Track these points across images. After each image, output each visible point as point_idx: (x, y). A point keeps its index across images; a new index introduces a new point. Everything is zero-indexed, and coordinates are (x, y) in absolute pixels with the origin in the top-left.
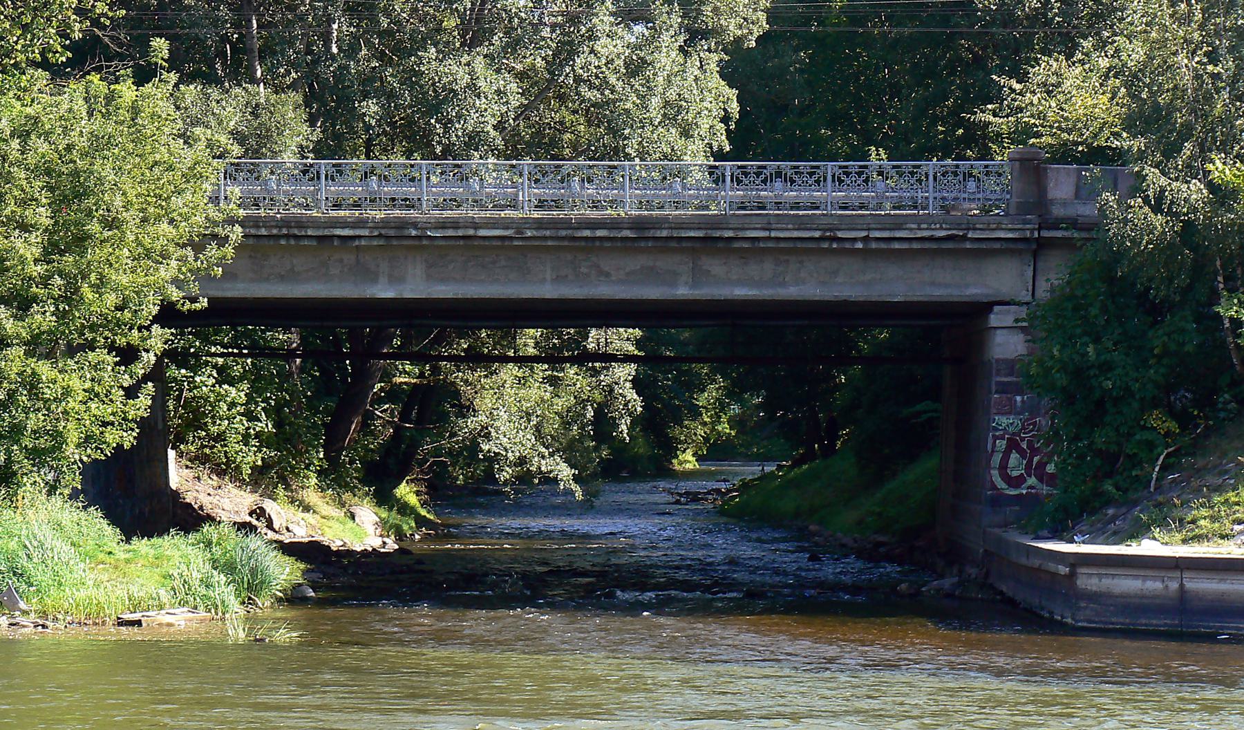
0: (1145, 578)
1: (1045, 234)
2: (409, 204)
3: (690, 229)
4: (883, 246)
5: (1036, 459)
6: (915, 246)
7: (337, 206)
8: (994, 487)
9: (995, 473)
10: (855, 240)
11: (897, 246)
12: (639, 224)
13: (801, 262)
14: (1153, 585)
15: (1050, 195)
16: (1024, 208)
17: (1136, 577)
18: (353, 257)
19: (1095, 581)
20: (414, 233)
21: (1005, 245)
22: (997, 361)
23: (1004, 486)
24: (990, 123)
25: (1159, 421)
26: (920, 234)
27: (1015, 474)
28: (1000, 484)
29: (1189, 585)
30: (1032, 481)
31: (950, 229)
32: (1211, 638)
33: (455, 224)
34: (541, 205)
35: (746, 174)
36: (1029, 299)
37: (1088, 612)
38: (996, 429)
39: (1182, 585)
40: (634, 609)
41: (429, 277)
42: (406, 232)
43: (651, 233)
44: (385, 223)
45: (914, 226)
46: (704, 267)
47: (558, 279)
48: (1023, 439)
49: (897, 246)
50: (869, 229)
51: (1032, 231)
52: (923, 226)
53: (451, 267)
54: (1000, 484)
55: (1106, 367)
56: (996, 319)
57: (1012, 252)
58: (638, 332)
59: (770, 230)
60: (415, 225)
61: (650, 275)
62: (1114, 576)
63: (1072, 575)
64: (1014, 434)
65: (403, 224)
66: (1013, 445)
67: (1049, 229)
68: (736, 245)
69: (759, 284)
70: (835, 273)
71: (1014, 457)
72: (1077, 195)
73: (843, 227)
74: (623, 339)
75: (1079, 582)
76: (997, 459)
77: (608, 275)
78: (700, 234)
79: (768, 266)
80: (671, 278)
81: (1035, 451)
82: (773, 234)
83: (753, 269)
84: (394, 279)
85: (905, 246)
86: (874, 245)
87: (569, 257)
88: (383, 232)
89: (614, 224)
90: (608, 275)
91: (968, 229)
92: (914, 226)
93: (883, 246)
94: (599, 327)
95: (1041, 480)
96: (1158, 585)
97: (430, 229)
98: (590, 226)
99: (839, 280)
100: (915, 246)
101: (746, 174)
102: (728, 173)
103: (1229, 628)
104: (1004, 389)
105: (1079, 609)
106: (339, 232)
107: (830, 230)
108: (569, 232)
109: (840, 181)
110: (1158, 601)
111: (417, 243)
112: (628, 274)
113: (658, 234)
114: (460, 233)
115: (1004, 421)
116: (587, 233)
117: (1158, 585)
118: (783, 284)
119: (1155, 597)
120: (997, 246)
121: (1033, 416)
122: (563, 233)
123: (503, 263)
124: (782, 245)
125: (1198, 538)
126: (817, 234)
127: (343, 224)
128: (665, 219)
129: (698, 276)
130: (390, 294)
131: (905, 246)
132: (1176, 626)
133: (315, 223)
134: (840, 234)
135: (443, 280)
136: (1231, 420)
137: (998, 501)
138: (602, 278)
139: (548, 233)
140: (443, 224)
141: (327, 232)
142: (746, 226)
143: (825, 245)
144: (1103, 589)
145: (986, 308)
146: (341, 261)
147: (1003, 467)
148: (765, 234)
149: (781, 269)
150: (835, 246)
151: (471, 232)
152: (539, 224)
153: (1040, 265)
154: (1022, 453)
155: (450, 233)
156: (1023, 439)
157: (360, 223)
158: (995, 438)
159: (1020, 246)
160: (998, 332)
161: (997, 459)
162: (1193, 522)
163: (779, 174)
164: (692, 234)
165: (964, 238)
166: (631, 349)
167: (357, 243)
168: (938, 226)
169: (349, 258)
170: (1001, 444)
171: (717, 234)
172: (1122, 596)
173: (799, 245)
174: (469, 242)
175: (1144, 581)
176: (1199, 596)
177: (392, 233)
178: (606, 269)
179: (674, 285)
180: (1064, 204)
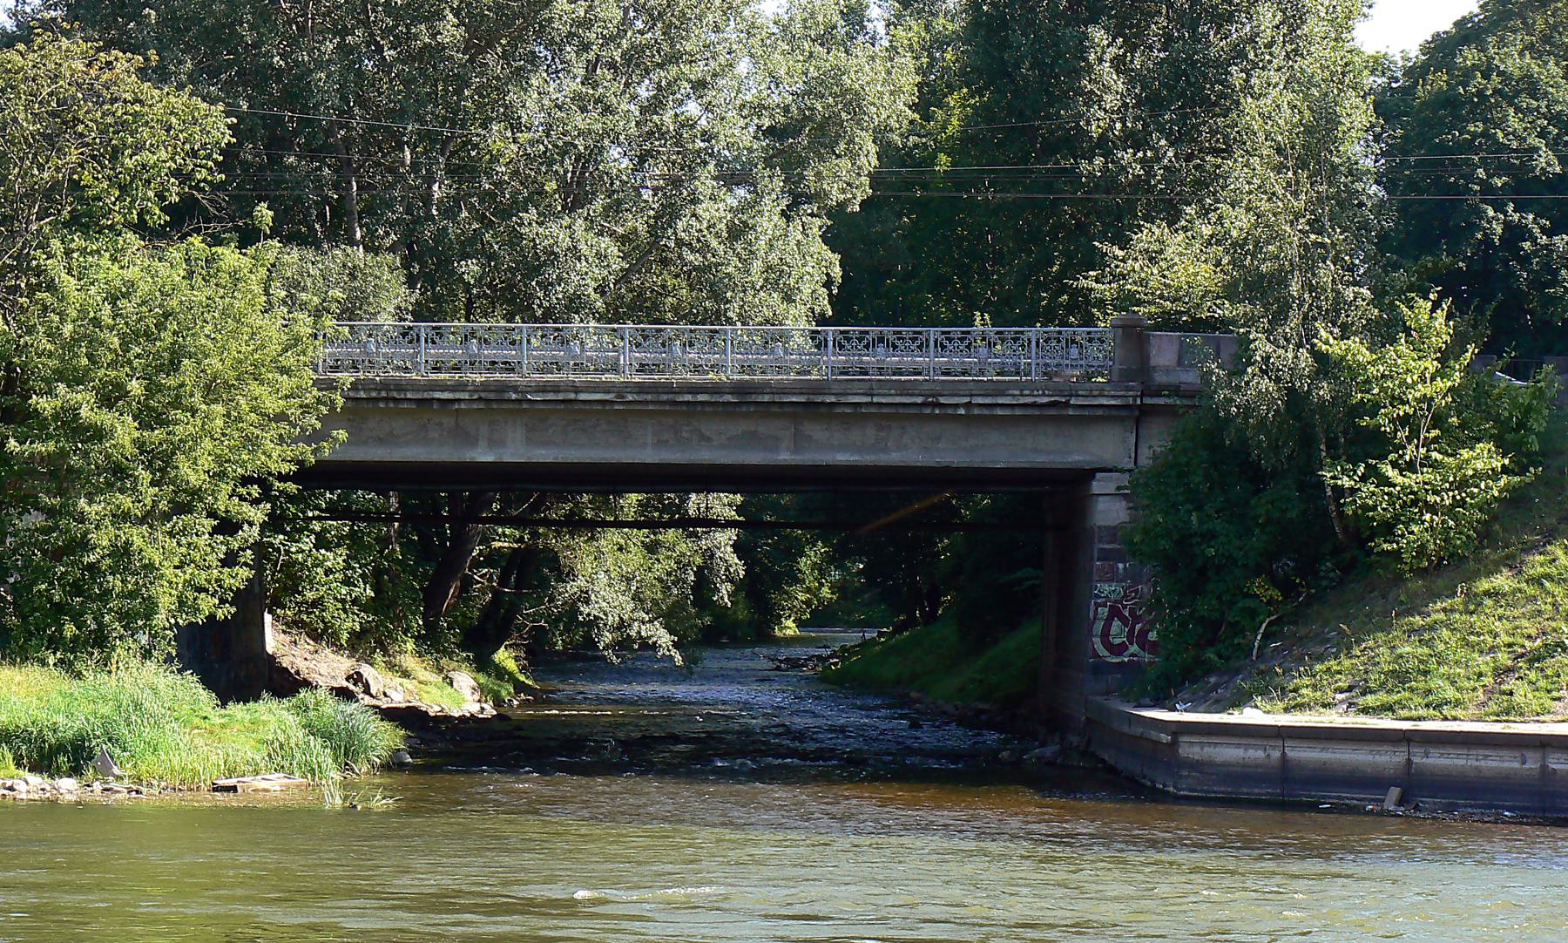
0: (1247, 747)
1: (1148, 401)
2: (509, 367)
4: (986, 412)
5: (1138, 627)
6: (1018, 412)
7: (436, 369)
8: (1095, 654)
9: (1097, 640)
10: (957, 406)
11: (999, 412)
12: (740, 389)
15: (1153, 362)
16: (1127, 375)
17: (1238, 746)
19: (1196, 749)
20: (514, 396)
21: (1107, 412)
23: (1106, 653)
25: (1261, 588)
26: (1022, 401)
27: (1117, 641)
28: (1102, 652)
29: (1291, 754)
30: (1134, 648)
31: (1052, 396)
32: (1313, 807)
33: (555, 388)
34: (642, 368)
36: (1131, 465)
38: (1098, 596)
39: (1284, 754)
41: (529, 441)
42: (506, 396)
43: (753, 398)
44: (485, 386)
46: (806, 433)
47: (660, 444)
48: (1125, 607)
49: (999, 412)
50: (971, 395)
51: (1135, 397)
52: (1027, 392)
53: (550, 431)
54: (1102, 652)
55: (1210, 536)
57: (1122, 420)
58: (739, 498)
59: (872, 395)
60: (515, 389)
61: (752, 439)
63: (1174, 744)
64: (1116, 601)
65: (503, 387)
66: (1115, 613)
67: (1151, 396)
68: (838, 410)
70: (938, 439)
71: (1116, 623)
72: (1180, 363)
73: (945, 393)
74: (723, 504)
75: (1180, 751)
76: (1099, 627)
77: (709, 439)
78: (802, 399)
79: (871, 432)
81: (1137, 619)
82: (875, 400)
83: (855, 435)
84: (494, 443)
85: (1008, 412)
86: (976, 411)
87: (671, 421)
88: (483, 395)
89: (715, 389)
90: (709, 439)
91: (1071, 396)
93: (986, 412)
94: (697, 492)
95: (1142, 648)
96: (1260, 754)
98: (693, 390)
100: (1018, 412)
103: (1330, 797)
104: (1105, 556)
105: (1181, 777)
106: (437, 395)
109: (943, 347)
112: (728, 439)
113: (760, 399)
114: (561, 396)
115: (1107, 588)
116: (688, 398)
117: (1260, 754)
118: (885, 450)
120: (1100, 412)
122: (665, 397)
125: (1300, 707)
126: (919, 400)
127: (442, 386)
128: (767, 384)
129: (799, 442)
130: (490, 459)
131: (1008, 412)
134: (942, 400)
135: (545, 444)
136: (1333, 588)
137: (1100, 668)
138: (703, 443)
140: (543, 388)
141: (426, 395)
142: (849, 391)
143: (928, 411)
144: (1206, 758)
146: (441, 424)
147: (1105, 635)
149: (883, 434)
150: (937, 412)
151: (572, 396)
152: (641, 388)
153: (1143, 432)
154: (1124, 620)
155: (550, 396)
156: (1125, 607)
157: (460, 386)
158: (1097, 605)
159: (1124, 413)
160: (1101, 499)
161: (1099, 627)
165: (1067, 404)
166: (731, 514)
168: (1040, 392)
169: (448, 421)
170: (1104, 612)
172: (1223, 765)
176: (1299, 764)
177: (492, 396)
180: (1167, 371)
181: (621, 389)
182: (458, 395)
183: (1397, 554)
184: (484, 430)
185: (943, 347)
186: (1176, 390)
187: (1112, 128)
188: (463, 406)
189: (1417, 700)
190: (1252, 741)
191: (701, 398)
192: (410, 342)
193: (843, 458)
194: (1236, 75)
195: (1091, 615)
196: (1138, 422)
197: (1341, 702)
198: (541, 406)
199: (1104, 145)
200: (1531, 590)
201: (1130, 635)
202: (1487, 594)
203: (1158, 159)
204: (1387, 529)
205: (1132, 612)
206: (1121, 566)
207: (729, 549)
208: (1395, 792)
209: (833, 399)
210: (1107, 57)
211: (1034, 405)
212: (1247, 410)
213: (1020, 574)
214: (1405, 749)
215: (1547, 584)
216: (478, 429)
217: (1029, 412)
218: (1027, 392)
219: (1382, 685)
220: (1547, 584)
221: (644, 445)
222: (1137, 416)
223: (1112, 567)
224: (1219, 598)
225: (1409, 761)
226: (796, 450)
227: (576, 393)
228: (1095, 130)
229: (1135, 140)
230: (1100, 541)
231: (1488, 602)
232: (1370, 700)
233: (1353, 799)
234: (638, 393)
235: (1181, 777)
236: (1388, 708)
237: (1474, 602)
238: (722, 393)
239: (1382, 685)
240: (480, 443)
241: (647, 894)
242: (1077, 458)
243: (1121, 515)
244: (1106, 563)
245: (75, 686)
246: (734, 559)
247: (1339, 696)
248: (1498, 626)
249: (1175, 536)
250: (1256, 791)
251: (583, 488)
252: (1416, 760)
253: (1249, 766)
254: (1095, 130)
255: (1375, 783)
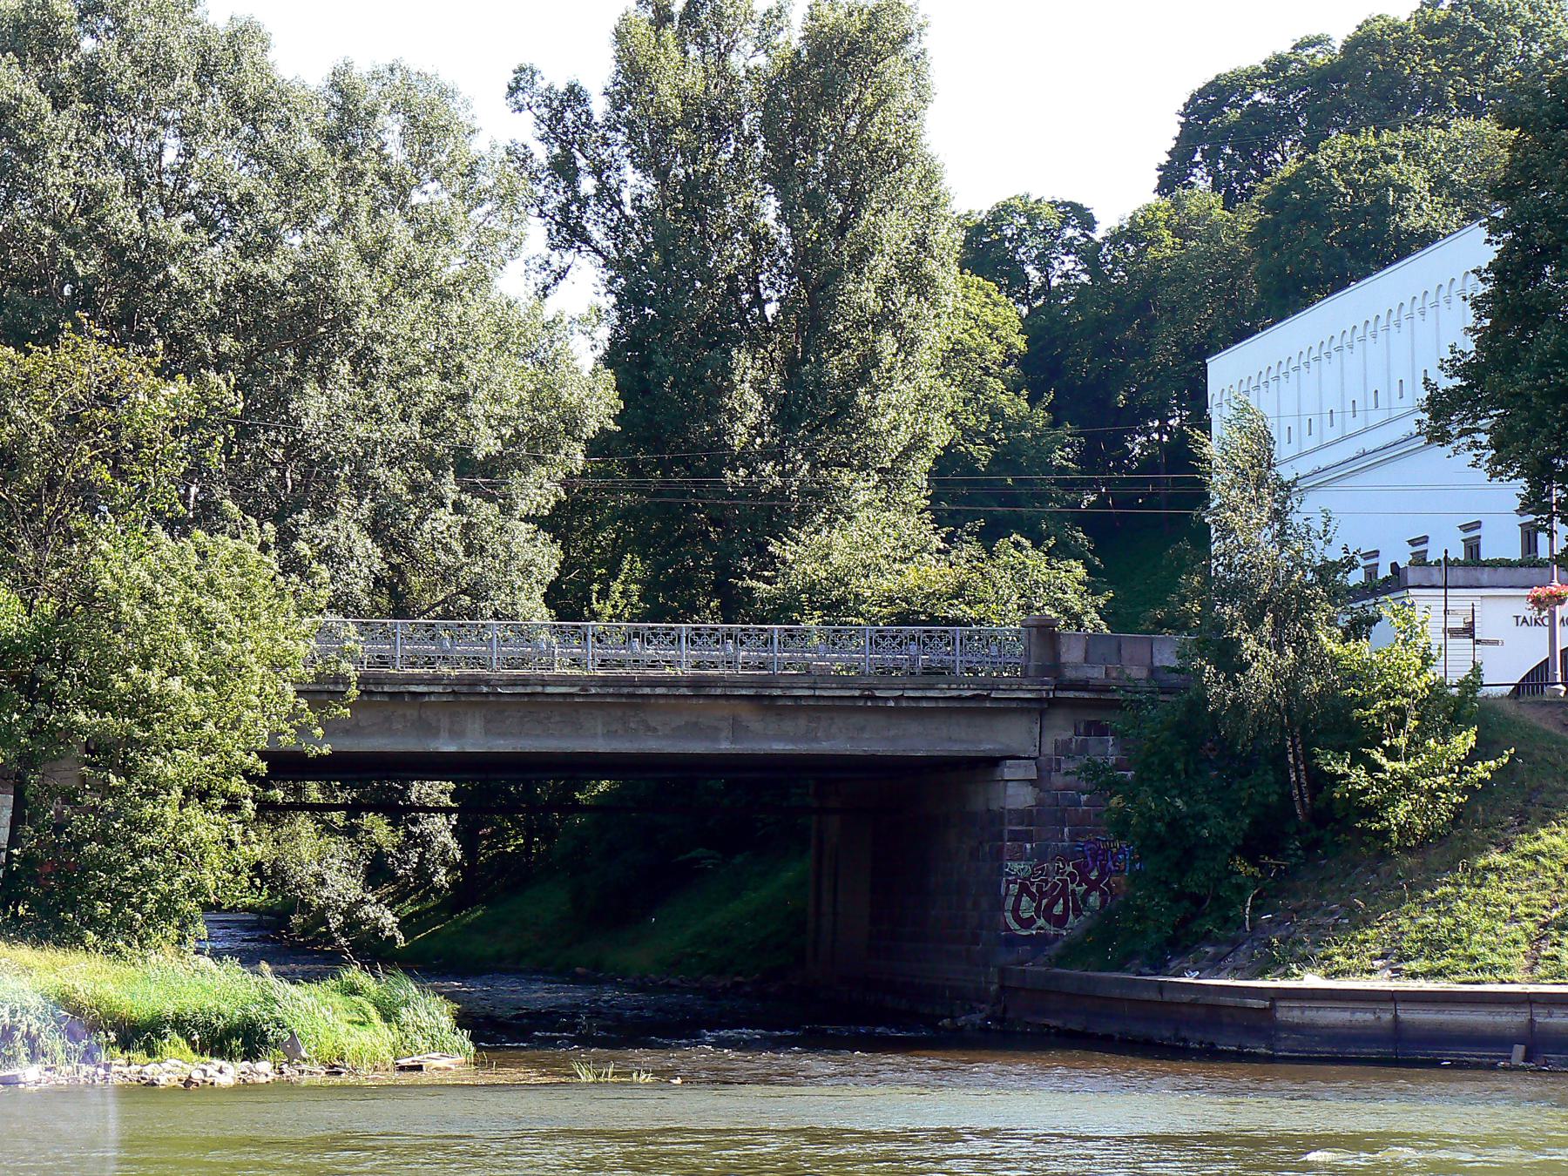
0: (1354, 1011)
1: (1059, 694)
2: (476, 661)
3: (742, 687)
4: (913, 704)
5: (1044, 902)
6: (941, 704)
7: (413, 665)
8: (1008, 928)
9: (1008, 915)
10: (887, 699)
11: (924, 704)
12: (696, 684)
13: (832, 719)
14: (1363, 1016)
15: (1063, 660)
16: (1043, 670)
17: (1344, 1010)
18: (416, 714)
19: (1297, 1013)
20: (485, 689)
21: (1020, 705)
22: (1009, 810)
23: (1017, 927)
24: (753, 589)
25: (1242, 867)
27: (1026, 915)
28: (1014, 926)
29: (1403, 1016)
30: (1041, 922)
32: (1434, 1064)
33: (525, 681)
34: (603, 664)
35: (655, 635)
36: (1036, 754)
37: (1289, 1042)
38: (1008, 874)
39: (1396, 1016)
40: (550, 1042)
41: (487, 732)
42: (478, 689)
43: (707, 691)
44: (460, 680)
45: (945, 686)
47: (611, 734)
48: (1032, 883)
49: (924, 704)
50: (904, 689)
51: (1048, 691)
52: (954, 686)
53: (508, 722)
54: (1014, 926)
55: (1202, 818)
56: (1010, 771)
57: (1029, 711)
58: (451, 786)
59: (814, 689)
60: (487, 683)
61: (695, 730)
62: (1318, 1008)
63: (1273, 1008)
64: (1025, 879)
65: (475, 681)
66: (1024, 889)
67: (1062, 690)
68: (780, 703)
69: (793, 740)
70: (863, 729)
71: (1025, 899)
72: (1086, 660)
74: (435, 791)
75: (1278, 1015)
76: (1010, 902)
77: (655, 730)
78: (751, 692)
79: (802, 722)
80: (713, 733)
81: (1043, 894)
82: (817, 693)
83: (788, 726)
84: (455, 734)
85: (932, 704)
86: (904, 704)
87: (619, 713)
88: (456, 689)
89: (674, 683)
91: (992, 690)
92: (945, 686)
93: (913, 704)
94: (422, 780)
95: (1048, 921)
96: (1369, 1017)
97: (500, 686)
99: (866, 736)
100: (941, 704)
101: (700, 636)
102: (776, 636)
103: (1447, 1055)
104: (1016, 837)
105: (1279, 1039)
106: (413, 688)
107: (868, 689)
108: (631, 690)
109: (877, 644)
110: (1369, 1031)
111: (484, 699)
112: (673, 729)
113: (713, 692)
114: (529, 690)
115: (1016, 866)
116: (647, 691)
117: (1369, 1017)
118: (816, 739)
119: (1365, 1027)
120: (1014, 705)
121: (1042, 861)
122: (625, 691)
123: (558, 718)
124: (822, 703)
125: (1336, 974)
126: (857, 693)
127: (420, 681)
128: (720, 678)
129: (738, 729)
130: (453, 749)
131: (932, 704)
132: (1392, 1054)
133: (392, 680)
134: (877, 693)
135: (503, 735)
136: (1303, 864)
137: (1012, 941)
139: (611, 690)
140: (513, 682)
141: (402, 689)
143: (861, 703)
144: (1307, 1020)
145: (993, 762)
146: (404, 716)
147: (1016, 910)
148: (807, 693)
150: (869, 704)
151: (539, 689)
152: (604, 682)
153: (1044, 722)
154: (1031, 895)
155: (519, 690)
156: (1032, 883)
157: (436, 680)
158: (1009, 883)
159: (1034, 705)
160: (1010, 784)
161: (1010, 902)
162: (1329, 958)
163: (730, 636)
164: (744, 692)
165: (987, 697)
166: (446, 800)
167: (427, 699)
169: (412, 713)
170: (1014, 888)
171: (767, 692)
172: (1327, 1027)
173: (837, 703)
174: (533, 699)
175: (1353, 1013)
176: (1412, 1025)
177: (465, 689)
178: (653, 724)
179: (716, 740)
180: (1076, 667)
181: (584, 683)
182: (432, 689)
183: (1385, 832)
184: (445, 722)
185: (877, 644)
186: (1083, 685)
187: (753, 443)
188: (433, 699)
189: (1463, 965)
190: (1357, 1005)
191: (659, 691)
192: (717, 642)
193: (779, 747)
194: (863, 399)
195: (1003, 891)
196: (1042, 714)
197: (1382, 968)
198: (507, 699)
199: (745, 459)
200: (1529, 865)
201: (1037, 909)
202: (1487, 869)
203: (794, 472)
204: (1371, 812)
205: (1039, 888)
206: (1028, 846)
207: (448, 834)
208: (1519, 1050)
209: (778, 692)
210: (748, 377)
211: (959, 698)
212: (1238, 707)
213: (693, 854)
214: (1393, 1006)
215: (1541, 859)
216: (439, 720)
217: (956, 704)
218: (954, 686)
219: (1420, 952)
220: (1541, 859)
221: (594, 736)
222: (1041, 708)
223: (1020, 846)
224: (1207, 874)
225: (1532, 1021)
226: (734, 740)
227: (543, 686)
228: (737, 443)
229: (774, 454)
230: (1010, 823)
231: (1492, 877)
232: (1414, 965)
233: (1484, 1056)
234: (600, 687)
235: (1279, 1039)
236: (1439, 973)
237: (1479, 877)
238: (679, 687)
239: (1420, 952)
240: (442, 733)
241: (731, 1152)
242: (988, 747)
243: (1028, 798)
244: (1016, 844)
245: (121, 968)
246: (453, 844)
247: (1377, 963)
248: (1514, 898)
249: (1167, 819)
250: (1365, 1050)
251: (413, 775)
252: (1538, 1020)
253: (1356, 1028)
254: (737, 443)
255: (1498, 1042)
